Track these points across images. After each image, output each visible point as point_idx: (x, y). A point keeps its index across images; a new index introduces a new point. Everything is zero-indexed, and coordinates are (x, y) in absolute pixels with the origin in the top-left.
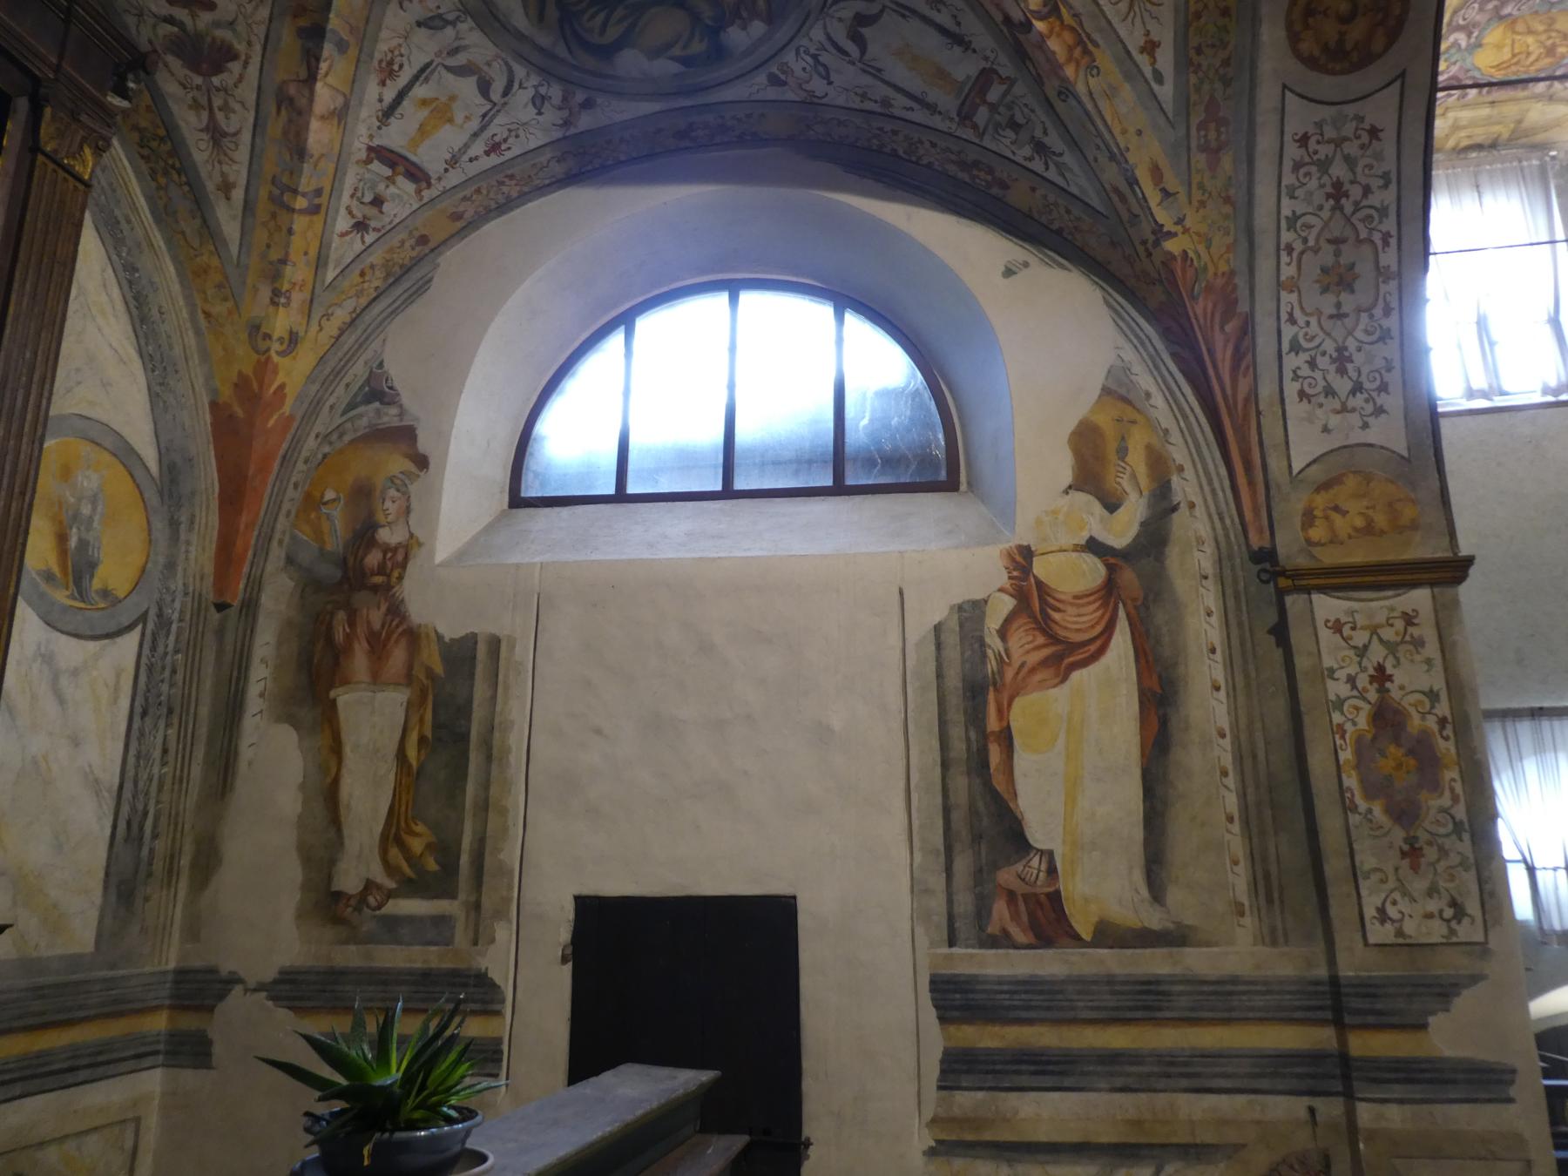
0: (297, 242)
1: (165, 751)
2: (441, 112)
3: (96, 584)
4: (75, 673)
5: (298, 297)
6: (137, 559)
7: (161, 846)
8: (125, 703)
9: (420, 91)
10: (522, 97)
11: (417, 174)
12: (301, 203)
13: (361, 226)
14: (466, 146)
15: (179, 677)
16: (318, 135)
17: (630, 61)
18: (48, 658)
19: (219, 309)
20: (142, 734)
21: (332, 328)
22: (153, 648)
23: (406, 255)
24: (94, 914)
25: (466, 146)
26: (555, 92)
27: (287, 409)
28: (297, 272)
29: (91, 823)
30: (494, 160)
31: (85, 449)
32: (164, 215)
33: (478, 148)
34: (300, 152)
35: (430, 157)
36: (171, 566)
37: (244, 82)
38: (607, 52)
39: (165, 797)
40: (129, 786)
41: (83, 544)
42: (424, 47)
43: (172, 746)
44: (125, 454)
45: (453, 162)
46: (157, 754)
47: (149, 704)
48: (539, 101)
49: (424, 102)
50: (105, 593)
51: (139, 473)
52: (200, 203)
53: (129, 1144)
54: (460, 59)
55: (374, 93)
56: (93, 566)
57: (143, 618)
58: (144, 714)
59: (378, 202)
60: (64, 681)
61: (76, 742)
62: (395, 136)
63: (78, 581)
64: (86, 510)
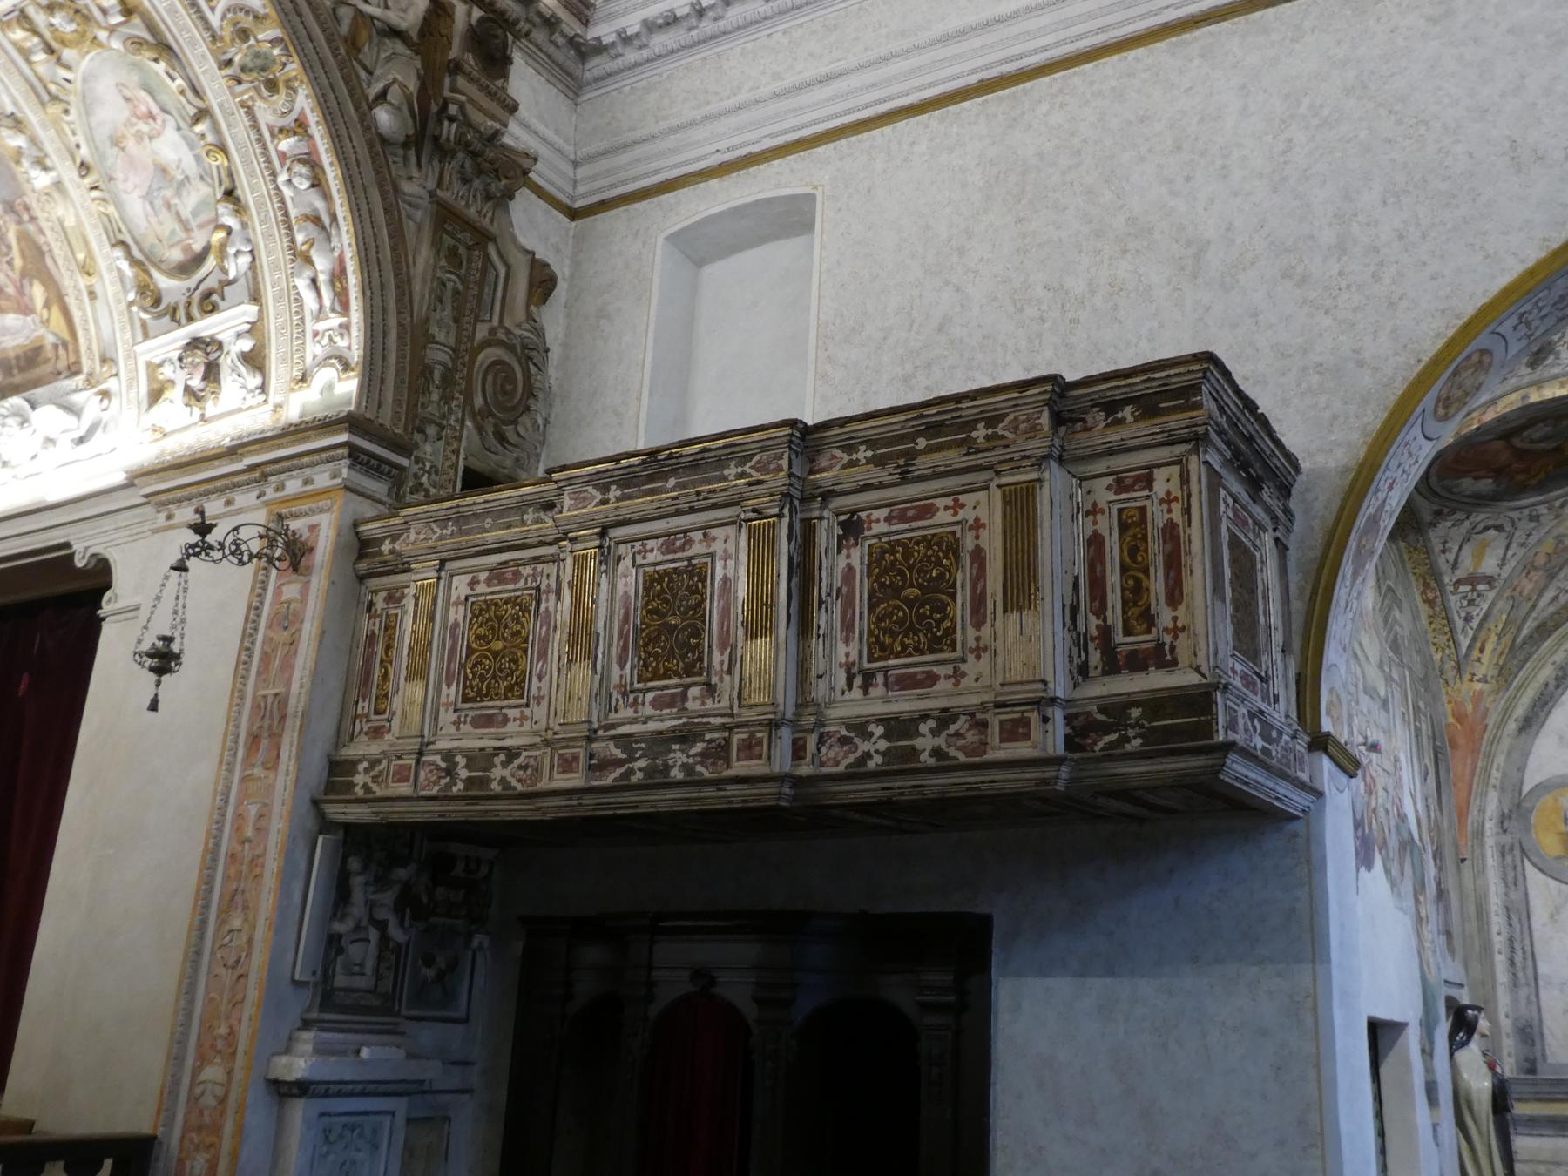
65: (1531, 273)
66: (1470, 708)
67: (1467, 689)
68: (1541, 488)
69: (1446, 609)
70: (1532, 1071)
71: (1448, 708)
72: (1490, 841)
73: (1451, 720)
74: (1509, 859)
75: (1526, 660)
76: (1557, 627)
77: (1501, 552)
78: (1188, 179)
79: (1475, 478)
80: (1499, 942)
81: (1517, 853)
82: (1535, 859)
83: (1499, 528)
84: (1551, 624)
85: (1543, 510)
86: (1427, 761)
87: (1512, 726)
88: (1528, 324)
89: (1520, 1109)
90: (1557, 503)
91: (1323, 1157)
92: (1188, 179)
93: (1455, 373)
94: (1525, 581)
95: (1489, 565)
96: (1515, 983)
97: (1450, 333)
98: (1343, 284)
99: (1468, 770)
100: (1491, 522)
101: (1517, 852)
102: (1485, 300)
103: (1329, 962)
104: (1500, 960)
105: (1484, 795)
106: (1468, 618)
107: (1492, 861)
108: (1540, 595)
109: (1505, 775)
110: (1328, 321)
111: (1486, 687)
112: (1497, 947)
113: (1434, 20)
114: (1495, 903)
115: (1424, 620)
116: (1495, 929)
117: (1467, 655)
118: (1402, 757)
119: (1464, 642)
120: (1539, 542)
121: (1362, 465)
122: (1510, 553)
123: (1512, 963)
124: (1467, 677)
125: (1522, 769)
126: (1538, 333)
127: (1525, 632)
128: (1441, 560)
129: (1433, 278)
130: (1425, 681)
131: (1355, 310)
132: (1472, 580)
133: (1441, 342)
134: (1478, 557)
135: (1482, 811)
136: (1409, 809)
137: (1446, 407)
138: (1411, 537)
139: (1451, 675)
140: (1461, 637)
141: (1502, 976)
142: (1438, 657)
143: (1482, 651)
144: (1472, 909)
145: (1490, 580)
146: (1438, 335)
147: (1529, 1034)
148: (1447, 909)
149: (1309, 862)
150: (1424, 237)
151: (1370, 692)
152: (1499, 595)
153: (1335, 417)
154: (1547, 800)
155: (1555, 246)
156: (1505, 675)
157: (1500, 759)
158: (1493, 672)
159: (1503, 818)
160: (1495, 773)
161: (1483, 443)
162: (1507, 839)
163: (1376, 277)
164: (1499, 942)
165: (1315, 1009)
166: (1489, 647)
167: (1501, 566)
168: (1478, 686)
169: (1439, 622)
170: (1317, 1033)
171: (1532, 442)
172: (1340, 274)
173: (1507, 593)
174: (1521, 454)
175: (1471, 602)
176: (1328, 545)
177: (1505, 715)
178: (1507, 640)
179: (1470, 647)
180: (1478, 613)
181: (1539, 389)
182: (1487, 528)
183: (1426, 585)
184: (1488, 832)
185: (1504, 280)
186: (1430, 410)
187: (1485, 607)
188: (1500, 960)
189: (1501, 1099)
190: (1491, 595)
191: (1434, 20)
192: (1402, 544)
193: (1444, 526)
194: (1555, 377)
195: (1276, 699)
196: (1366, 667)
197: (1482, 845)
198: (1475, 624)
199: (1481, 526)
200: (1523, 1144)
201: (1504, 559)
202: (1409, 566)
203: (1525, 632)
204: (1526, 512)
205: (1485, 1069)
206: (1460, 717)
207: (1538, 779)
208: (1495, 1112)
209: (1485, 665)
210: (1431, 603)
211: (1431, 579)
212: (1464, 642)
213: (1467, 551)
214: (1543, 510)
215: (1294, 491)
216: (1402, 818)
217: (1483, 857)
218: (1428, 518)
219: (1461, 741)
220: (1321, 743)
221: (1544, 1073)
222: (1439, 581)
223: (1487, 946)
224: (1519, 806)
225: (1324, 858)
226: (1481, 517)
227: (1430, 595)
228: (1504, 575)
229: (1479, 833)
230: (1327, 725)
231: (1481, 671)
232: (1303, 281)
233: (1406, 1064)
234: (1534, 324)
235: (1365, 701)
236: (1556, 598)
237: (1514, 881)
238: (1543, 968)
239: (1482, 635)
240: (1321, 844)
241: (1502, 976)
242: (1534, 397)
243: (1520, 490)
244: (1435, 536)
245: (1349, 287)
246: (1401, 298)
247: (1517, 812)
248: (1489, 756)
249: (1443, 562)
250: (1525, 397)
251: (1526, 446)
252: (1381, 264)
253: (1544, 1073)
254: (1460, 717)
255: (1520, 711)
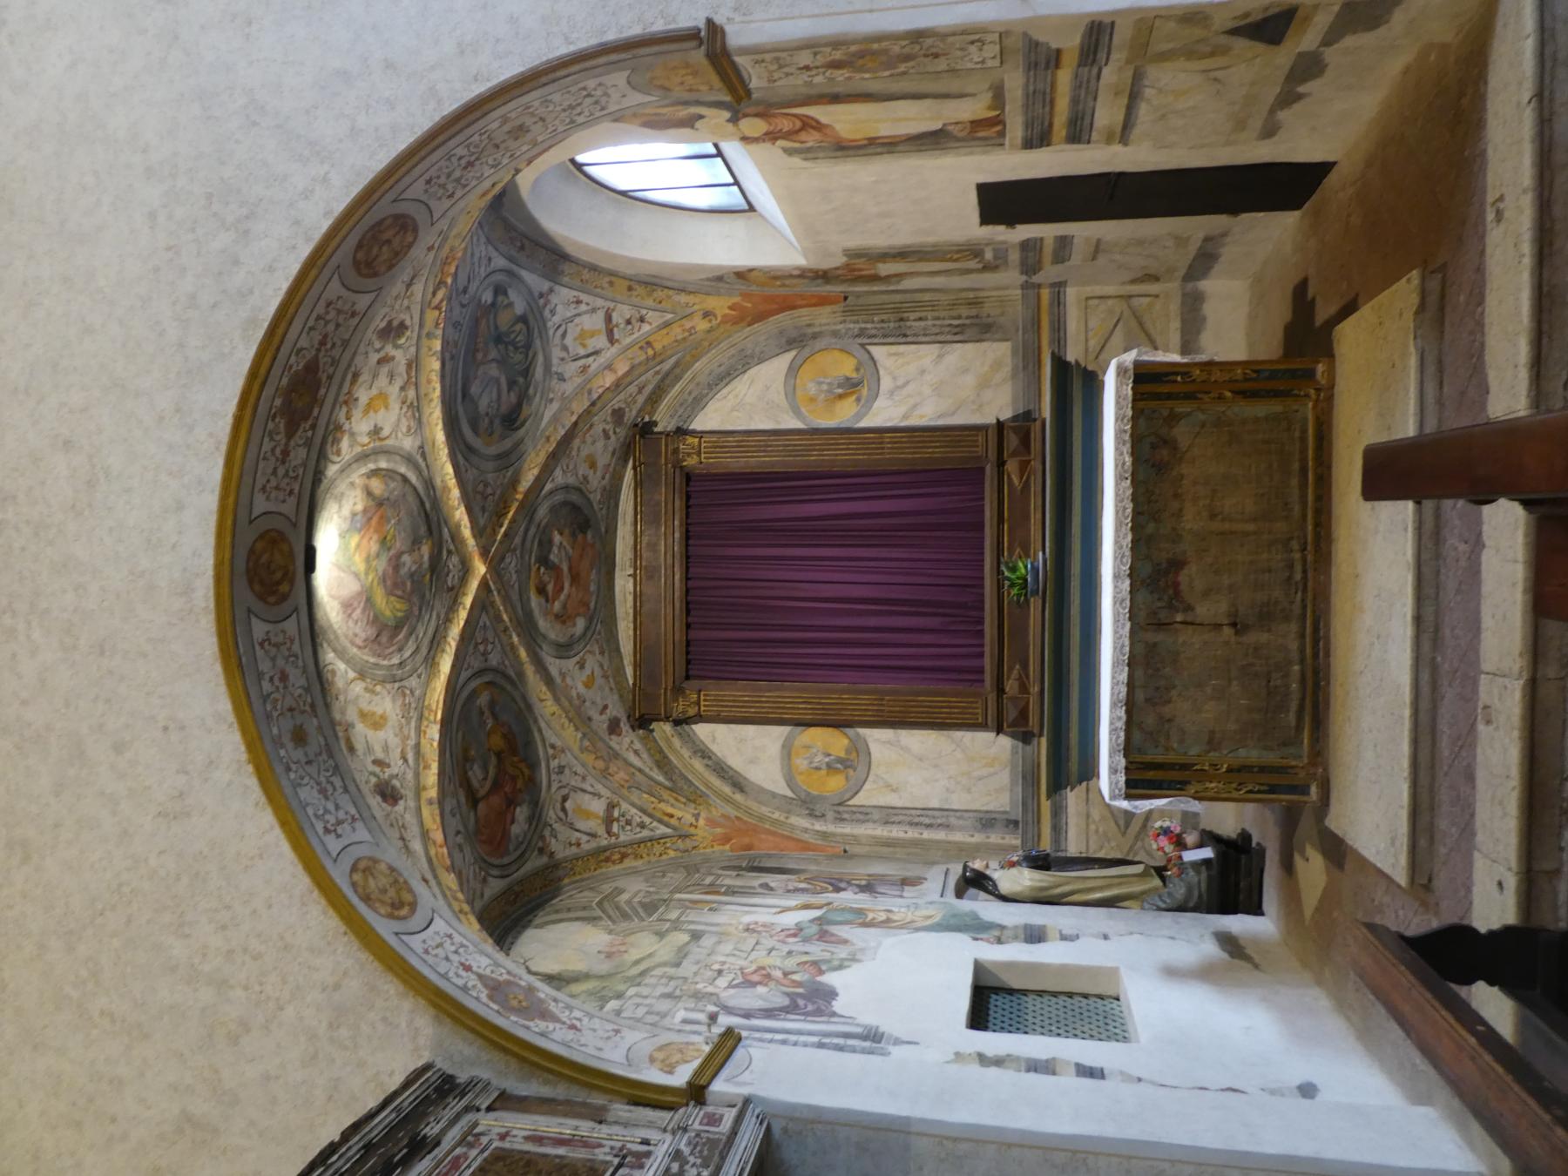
0: (666, 341)
1: (920, 319)
2: (582, 337)
3: (854, 375)
4: (895, 378)
5: (688, 325)
6: (837, 354)
7: (965, 312)
8: (902, 348)
9: (582, 352)
10: (556, 319)
11: (608, 318)
12: (650, 352)
13: (642, 320)
14: (586, 312)
15: (885, 317)
16: (622, 368)
17: (520, 308)
18: (891, 393)
19: (706, 344)
20: (915, 335)
21: (690, 299)
22: (874, 336)
23: (640, 290)
24: (995, 345)
25: (586, 312)
26: (547, 313)
27: (737, 299)
28: (677, 332)
29: (960, 354)
30: (583, 297)
31: (799, 393)
32: (678, 378)
33: (583, 307)
34: (633, 368)
35: (597, 321)
36: (835, 334)
37: (616, 403)
38: (523, 319)
39: (942, 314)
40: (940, 338)
41: (839, 386)
42: (571, 369)
43: (918, 315)
44: (793, 371)
45: (594, 310)
46: (922, 324)
47: (901, 335)
48: (553, 312)
49: (584, 346)
50: (857, 370)
51: (798, 362)
52: (667, 374)
53: (1096, 302)
54: (564, 354)
55: (595, 364)
56: (848, 379)
57: (863, 345)
58: (905, 336)
59: (628, 322)
60: (900, 383)
61: (923, 372)
62: (601, 341)
63: (857, 385)
64: (825, 387)
65: (284, 824)
66: (719, 830)
67: (703, 831)
68: (533, 766)
69: (631, 844)
70: (1016, 823)
71: (717, 848)
72: (831, 828)
73: (727, 847)
74: (846, 816)
75: (686, 779)
76: (661, 751)
77: (587, 797)
78: (113, 1120)
79: (513, 822)
80: (912, 834)
81: (842, 809)
82: (847, 796)
83: (565, 799)
84: (658, 757)
85: (554, 764)
86: (756, 883)
87: (738, 797)
88: (339, 823)
89: (1046, 845)
90: (551, 751)
91: (1096, 1154)
92: (113, 1120)
93: (366, 899)
94: (617, 777)
95: (598, 807)
96: (947, 826)
97: (323, 902)
98: (257, 988)
99: (771, 838)
100: (558, 805)
101: (841, 809)
102: (300, 867)
103: (908, 1118)
104: (927, 835)
105: (793, 827)
106: (642, 826)
107: (847, 829)
108: (631, 765)
109: (778, 808)
110: (290, 1011)
111: (703, 815)
112: (916, 835)
113: (26, 859)
114: (881, 831)
115: (639, 863)
116: (902, 835)
117: (675, 829)
118: (747, 919)
119: (663, 830)
120: (583, 766)
121: (436, 1006)
122: (589, 789)
123: (929, 826)
124: (692, 830)
125: (774, 795)
126: (353, 811)
127: (661, 778)
128: (586, 847)
129: (270, 907)
130: (691, 869)
131: (284, 982)
132: (609, 821)
133: (331, 912)
134: (588, 815)
135: (806, 830)
136: (791, 919)
137: (401, 905)
138: (560, 873)
139: (689, 843)
140: (658, 832)
141: (940, 835)
142: (672, 853)
143: (672, 816)
144: (886, 850)
145: (611, 806)
146: (325, 913)
147: (987, 821)
148: (883, 879)
149: (812, 1122)
150: (228, 907)
151: (682, 954)
152: (626, 799)
153: (384, 1019)
154: (800, 779)
155: (263, 799)
156: (695, 797)
157: (765, 810)
158: (691, 808)
159: (812, 815)
160: (776, 815)
161: (477, 822)
162: (830, 815)
163: (257, 957)
164: (912, 834)
165: (955, 1140)
166: (670, 810)
167: (600, 796)
168: (701, 822)
169: (642, 850)
170: (977, 1141)
171: (485, 779)
172: (246, 988)
173: (625, 792)
174: (496, 786)
175: (628, 823)
176: (505, 1050)
177: (728, 800)
178: (666, 795)
179: (667, 825)
180: (638, 817)
181: (425, 788)
182: (564, 810)
183: (607, 860)
184: (824, 828)
185: (286, 847)
186: (396, 926)
187: (634, 811)
188: (927, 835)
189: (1040, 862)
190: (624, 806)
191: (26, 859)
192: (566, 881)
193: (554, 845)
194: (417, 775)
195: (646, 1142)
196: (657, 959)
197: (834, 835)
198: (647, 820)
199: (561, 815)
200: (1073, 848)
201: (594, 794)
202: (586, 875)
203: (661, 778)
204: (554, 777)
205: (1014, 871)
206: (726, 839)
207: (783, 783)
208: (1048, 869)
209: (684, 814)
210: (624, 856)
211: (602, 856)
212: (663, 830)
213: (581, 825)
214: (554, 764)
215: (450, 1072)
216: (798, 931)
217: (842, 835)
218: (545, 859)
219: (746, 840)
220: (696, 1092)
221: (1018, 814)
222: (605, 849)
223: (915, 843)
224: (804, 802)
225: (809, 1107)
226: (551, 815)
227: (617, 857)
228: (609, 794)
229: (824, 835)
230: (680, 1078)
231: (689, 818)
232: (245, 1026)
233: (1011, 966)
234: (341, 815)
235: (688, 968)
236: (636, 752)
237: (864, 815)
238: (935, 804)
239: (658, 815)
240: (794, 1107)
241: (940, 835)
242: (433, 793)
243: (532, 783)
244: (560, 850)
245: (261, 984)
246: (282, 938)
247: (809, 805)
248: (762, 818)
249: (588, 845)
250: (430, 802)
251: (488, 784)
252: (245, 950)
253: (1018, 814)
254: (726, 839)
255: (727, 790)
